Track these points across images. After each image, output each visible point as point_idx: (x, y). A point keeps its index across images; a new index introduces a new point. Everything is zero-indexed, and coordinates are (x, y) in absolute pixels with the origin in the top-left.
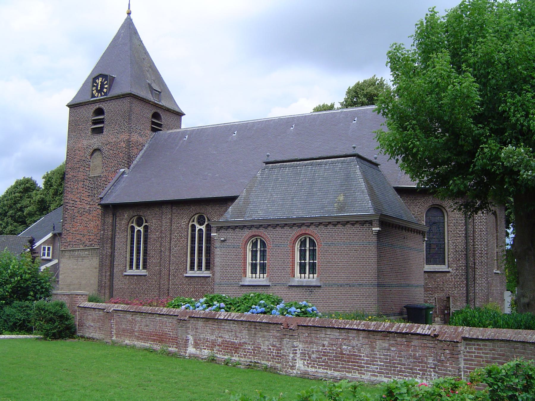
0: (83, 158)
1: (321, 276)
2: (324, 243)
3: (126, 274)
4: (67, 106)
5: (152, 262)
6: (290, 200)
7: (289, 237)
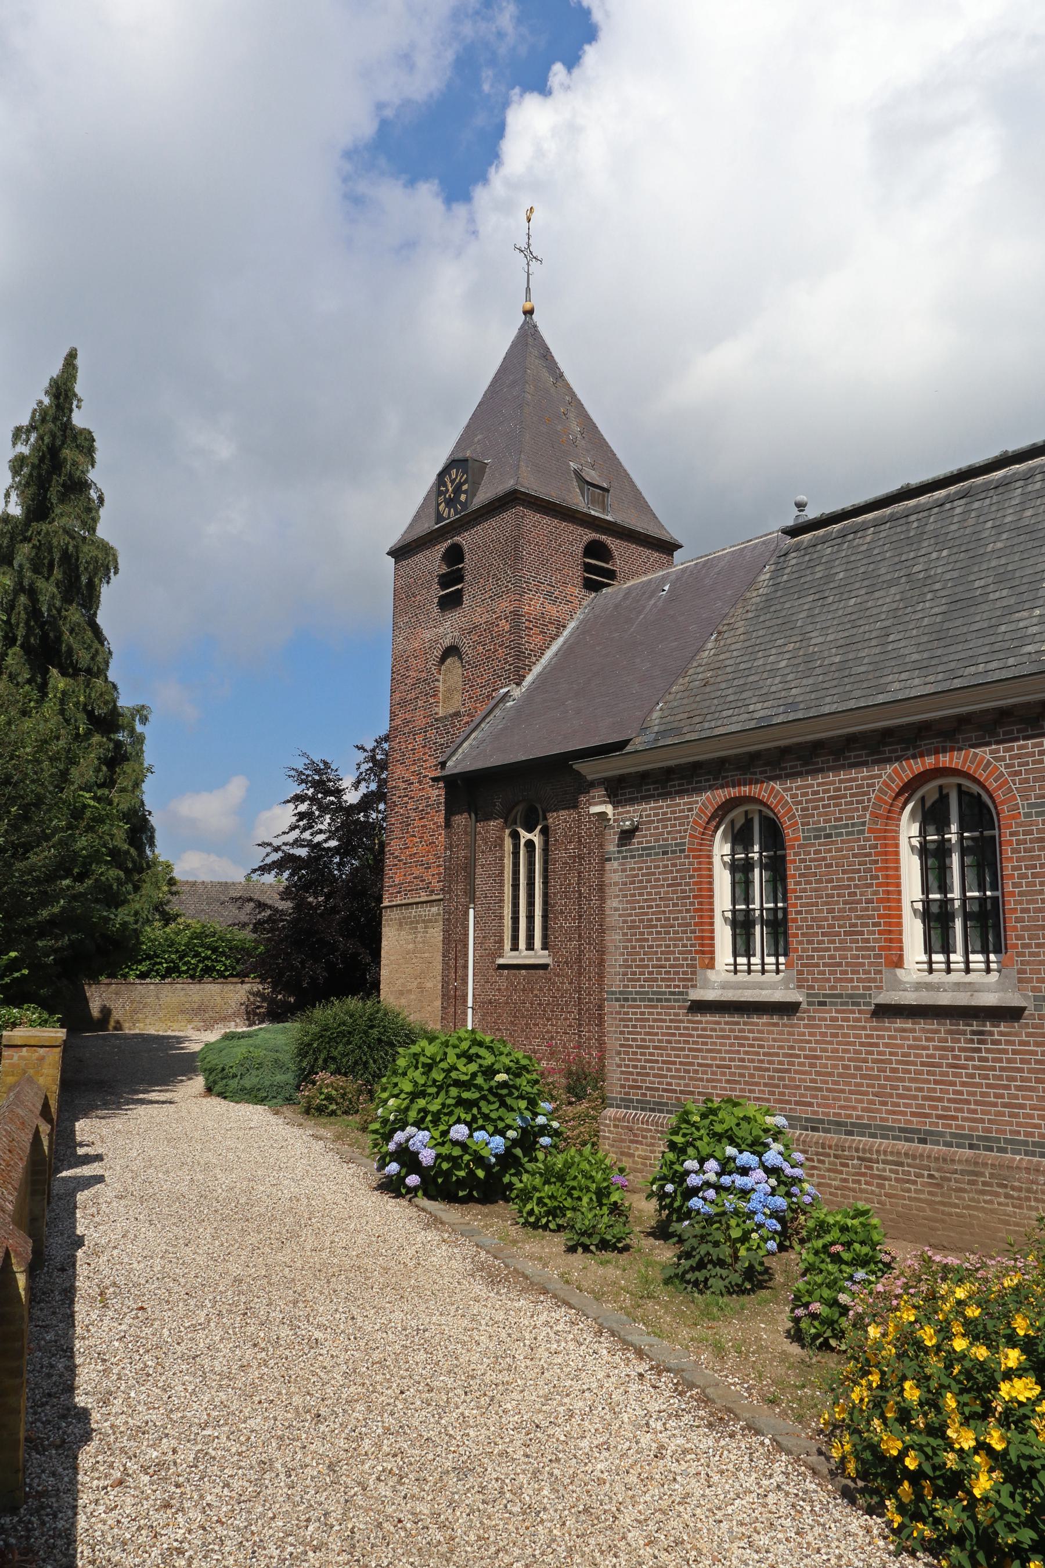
0: (424, 675)
1: (1022, 963)
2: (1030, 806)
3: (501, 961)
4: (388, 554)
5: (561, 927)
6: (874, 643)
7: (867, 793)
